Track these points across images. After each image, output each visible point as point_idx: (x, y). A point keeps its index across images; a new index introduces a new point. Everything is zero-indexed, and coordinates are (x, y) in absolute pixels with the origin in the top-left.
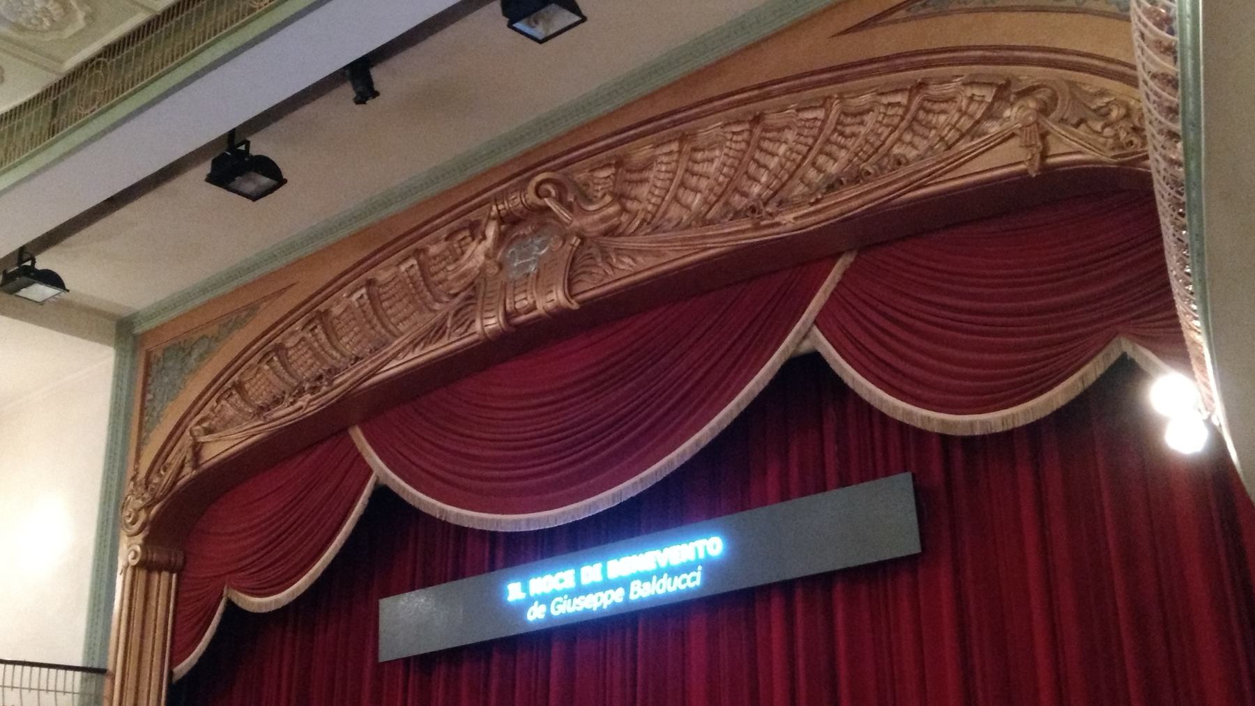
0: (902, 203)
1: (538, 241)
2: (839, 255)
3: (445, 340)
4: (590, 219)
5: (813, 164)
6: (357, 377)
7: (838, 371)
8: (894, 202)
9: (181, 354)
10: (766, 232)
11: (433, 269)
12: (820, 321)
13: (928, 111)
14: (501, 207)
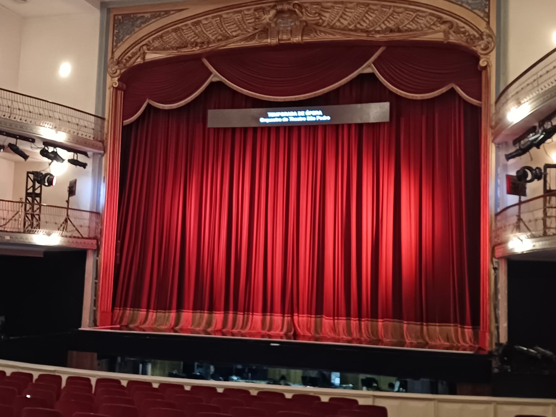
1: (290, 20)
12: (374, 63)
13: (418, 18)
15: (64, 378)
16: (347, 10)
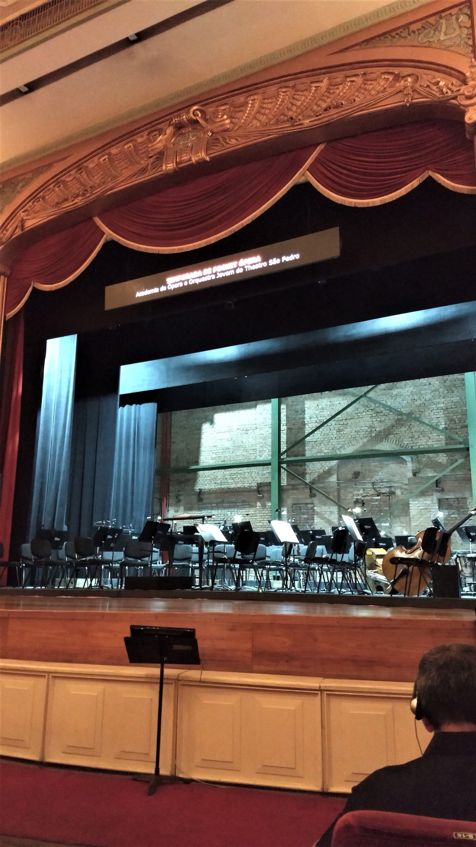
0: (354, 117)
2: (318, 144)
3: (147, 174)
4: (217, 125)
5: (316, 104)
6: (104, 190)
7: (315, 187)
8: (348, 117)
9: (13, 186)
10: (296, 128)
11: (140, 148)
14: (176, 119)
15: (107, 610)
16: (266, 101)
